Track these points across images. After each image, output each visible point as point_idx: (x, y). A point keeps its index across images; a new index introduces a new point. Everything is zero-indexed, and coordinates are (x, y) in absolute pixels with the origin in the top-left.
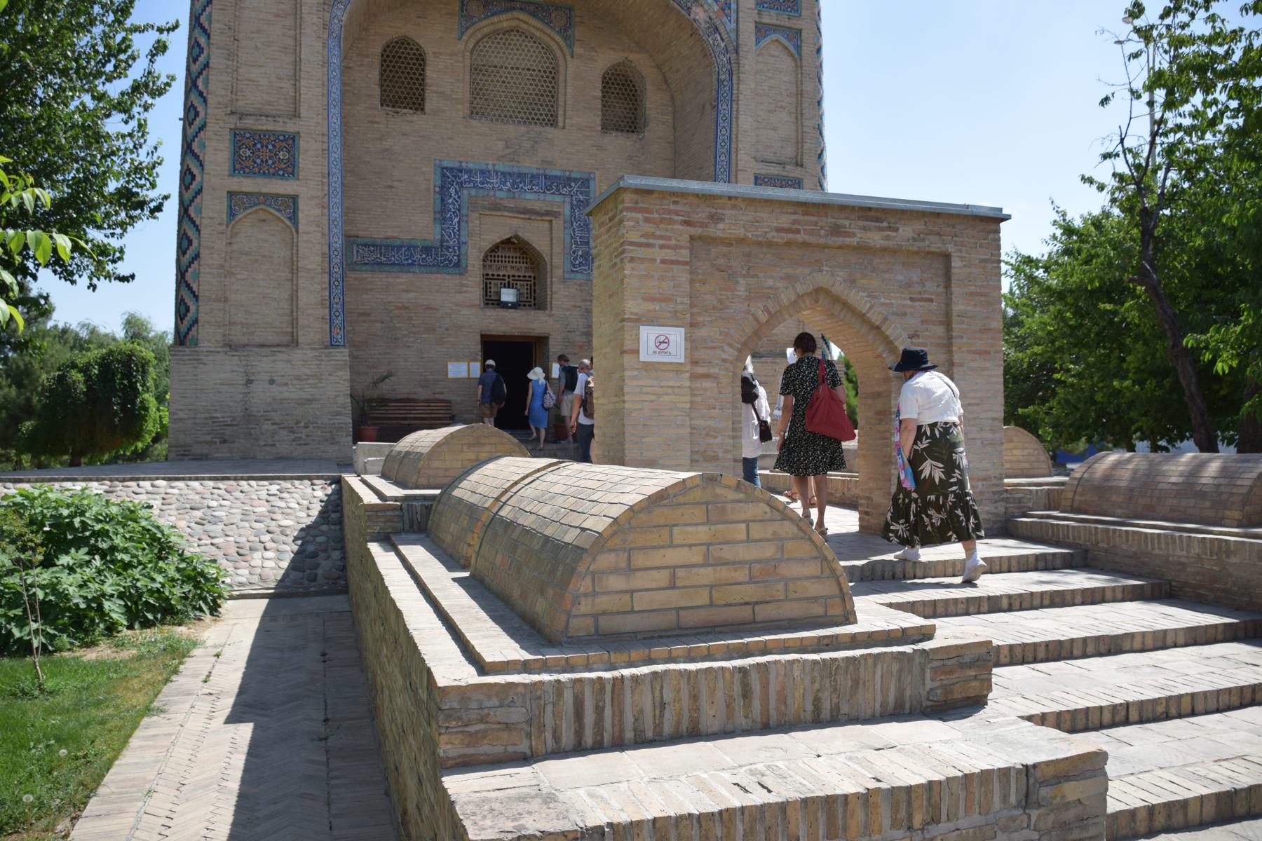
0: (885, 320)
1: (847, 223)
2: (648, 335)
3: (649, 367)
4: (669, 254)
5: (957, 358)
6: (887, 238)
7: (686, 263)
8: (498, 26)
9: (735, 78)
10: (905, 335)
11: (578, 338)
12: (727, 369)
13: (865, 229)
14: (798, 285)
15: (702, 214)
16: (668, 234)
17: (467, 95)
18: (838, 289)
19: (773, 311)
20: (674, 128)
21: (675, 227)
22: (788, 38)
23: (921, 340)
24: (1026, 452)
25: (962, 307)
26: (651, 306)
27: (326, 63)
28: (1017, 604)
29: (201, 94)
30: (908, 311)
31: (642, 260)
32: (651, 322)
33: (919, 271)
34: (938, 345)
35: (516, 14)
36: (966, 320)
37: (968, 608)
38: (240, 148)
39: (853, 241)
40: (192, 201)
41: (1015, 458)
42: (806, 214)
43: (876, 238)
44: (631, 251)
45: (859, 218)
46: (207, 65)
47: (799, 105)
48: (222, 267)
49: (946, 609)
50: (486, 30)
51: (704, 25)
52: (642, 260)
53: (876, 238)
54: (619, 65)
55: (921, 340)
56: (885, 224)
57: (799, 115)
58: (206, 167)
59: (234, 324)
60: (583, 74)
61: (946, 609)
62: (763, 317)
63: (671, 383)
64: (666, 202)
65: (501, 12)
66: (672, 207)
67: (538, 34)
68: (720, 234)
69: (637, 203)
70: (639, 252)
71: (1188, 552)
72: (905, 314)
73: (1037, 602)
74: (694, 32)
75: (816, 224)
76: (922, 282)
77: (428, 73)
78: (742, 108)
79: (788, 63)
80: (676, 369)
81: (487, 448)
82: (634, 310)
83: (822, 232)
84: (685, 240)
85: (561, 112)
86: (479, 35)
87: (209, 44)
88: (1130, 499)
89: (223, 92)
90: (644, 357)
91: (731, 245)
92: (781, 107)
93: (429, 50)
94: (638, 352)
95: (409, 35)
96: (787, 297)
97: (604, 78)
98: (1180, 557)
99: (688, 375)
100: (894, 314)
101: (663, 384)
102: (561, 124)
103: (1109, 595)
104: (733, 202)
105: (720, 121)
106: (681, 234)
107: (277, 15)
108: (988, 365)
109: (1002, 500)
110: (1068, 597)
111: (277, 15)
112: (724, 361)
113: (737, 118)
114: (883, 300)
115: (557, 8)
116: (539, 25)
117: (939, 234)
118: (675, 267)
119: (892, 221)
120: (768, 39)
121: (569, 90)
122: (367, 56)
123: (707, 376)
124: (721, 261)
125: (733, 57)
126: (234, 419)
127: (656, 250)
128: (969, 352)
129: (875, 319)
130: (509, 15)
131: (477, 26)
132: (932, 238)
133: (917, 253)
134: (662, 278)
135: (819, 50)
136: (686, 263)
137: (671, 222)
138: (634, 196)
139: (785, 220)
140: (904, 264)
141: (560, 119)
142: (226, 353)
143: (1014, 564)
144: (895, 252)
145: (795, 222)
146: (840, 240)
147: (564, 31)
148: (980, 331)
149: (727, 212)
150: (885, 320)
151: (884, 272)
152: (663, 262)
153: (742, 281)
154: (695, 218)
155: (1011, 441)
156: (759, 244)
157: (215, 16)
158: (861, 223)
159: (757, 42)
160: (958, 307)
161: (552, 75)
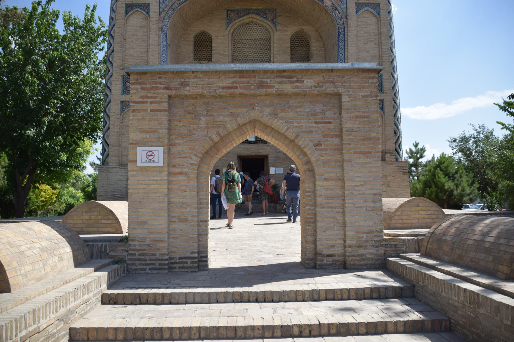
0: (297, 136)
1: (269, 80)
2: (141, 152)
3: (143, 169)
4: (155, 106)
5: (346, 157)
6: (296, 87)
7: (165, 111)
8: (244, 21)
9: (346, 30)
10: (311, 144)
11: (281, 156)
12: (194, 169)
13: (281, 83)
14: (239, 119)
15: (176, 82)
16: (155, 95)
17: (230, 53)
18: (266, 119)
19: (222, 134)
20: (325, 58)
21: (159, 91)
22: (373, 8)
23: (323, 147)
24: (429, 213)
25: (349, 126)
26: (144, 136)
27: (160, 44)
28: (307, 332)
29: (111, 62)
30: (313, 130)
31: (139, 111)
32: (144, 144)
33: (321, 106)
34: (335, 150)
35: (251, 15)
36: (352, 133)
37: (263, 333)
38: (125, 83)
39: (274, 90)
40: (107, 106)
41: (422, 216)
42: (241, 77)
43: (288, 88)
44: (134, 106)
45: (277, 77)
46: (113, 51)
47: (380, 39)
48: (118, 132)
49: (245, 333)
50: (238, 24)
51: (330, 8)
52: (139, 111)
53: (288, 88)
54: (298, 32)
55: (323, 147)
56: (295, 79)
57: (380, 44)
58: (112, 91)
59: (124, 155)
60: (282, 37)
61: (245, 333)
62: (216, 139)
63: (156, 178)
64: (154, 78)
65: (244, 15)
66: (158, 80)
67: (261, 23)
68: (186, 93)
69: (137, 80)
70: (138, 106)
71: (459, 299)
72: (311, 132)
73: (325, 330)
74: (327, 12)
75: (248, 82)
76: (323, 112)
77: (213, 45)
78: (349, 44)
79: (373, 20)
80: (158, 170)
81: (95, 213)
82: (134, 139)
83: (252, 87)
84: (165, 98)
85: (272, 56)
86: (235, 26)
87: (114, 42)
88: (452, 250)
89: (119, 61)
90: (139, 164)
91: (197, 99)
92: (371, 41)
93: (213, 35)
94: (136, 161)
95: (205, 30)
96: (231, 126)
97: (291, 38)
98: (455, 301)
99: (166, 173)
100: (303, 132)
101: (151, 178)
102: (272, 61)
103: (391, 328)
104: (195, 74)
105: (339, 51)
106: (164, 94)
107: (141, 27)
108: (369, 160)
109: (382, 246)
110: (353, 329)
111: (141, 27)
112: (191, 164)
113: (347, 48)
114: (295, 124)
115: (269, 10)
116: (261, 19)
117: (333, 82)
118: (159, 113)
119: (299, 76)
120: (363, 10)
121: (275, 45)
122: (187, 41)
123: (181, 173)
124: (191, 108)
125: (345, 20)
126: (122, 195)
127: (148, 104)
128: (354, 153)
129: (290, 135)
130: (248, 16)
131: (234, 23)
132: (328, 85)
133: (319, 95)
134: (151, 120)
135: (390, 12)
136: (165, 111)
137: (157, 88)
138: (136, 76)
139: (228, 82)
140: (310, 102)
141: (272, 59)
142: (119, 167)
143: (352, 294)
144: (304, 95)
145: (234, 82)
146: (264, 91)
147: (273, 21)
148: (363, 140)
149: (191, 80)
150: (297, 136)
151: (297, 107)
152: (152, 111)
153: (203, 119)
154: (171, 85)
155: (418, 206)
156: (214, 97)
157: (116, 31)
158: (279, 80)
159: (357, 12)
160: (345, 126)
161: (269, 40)
